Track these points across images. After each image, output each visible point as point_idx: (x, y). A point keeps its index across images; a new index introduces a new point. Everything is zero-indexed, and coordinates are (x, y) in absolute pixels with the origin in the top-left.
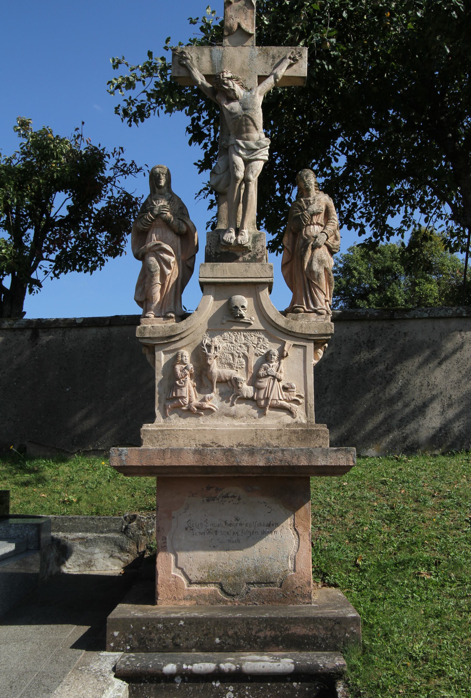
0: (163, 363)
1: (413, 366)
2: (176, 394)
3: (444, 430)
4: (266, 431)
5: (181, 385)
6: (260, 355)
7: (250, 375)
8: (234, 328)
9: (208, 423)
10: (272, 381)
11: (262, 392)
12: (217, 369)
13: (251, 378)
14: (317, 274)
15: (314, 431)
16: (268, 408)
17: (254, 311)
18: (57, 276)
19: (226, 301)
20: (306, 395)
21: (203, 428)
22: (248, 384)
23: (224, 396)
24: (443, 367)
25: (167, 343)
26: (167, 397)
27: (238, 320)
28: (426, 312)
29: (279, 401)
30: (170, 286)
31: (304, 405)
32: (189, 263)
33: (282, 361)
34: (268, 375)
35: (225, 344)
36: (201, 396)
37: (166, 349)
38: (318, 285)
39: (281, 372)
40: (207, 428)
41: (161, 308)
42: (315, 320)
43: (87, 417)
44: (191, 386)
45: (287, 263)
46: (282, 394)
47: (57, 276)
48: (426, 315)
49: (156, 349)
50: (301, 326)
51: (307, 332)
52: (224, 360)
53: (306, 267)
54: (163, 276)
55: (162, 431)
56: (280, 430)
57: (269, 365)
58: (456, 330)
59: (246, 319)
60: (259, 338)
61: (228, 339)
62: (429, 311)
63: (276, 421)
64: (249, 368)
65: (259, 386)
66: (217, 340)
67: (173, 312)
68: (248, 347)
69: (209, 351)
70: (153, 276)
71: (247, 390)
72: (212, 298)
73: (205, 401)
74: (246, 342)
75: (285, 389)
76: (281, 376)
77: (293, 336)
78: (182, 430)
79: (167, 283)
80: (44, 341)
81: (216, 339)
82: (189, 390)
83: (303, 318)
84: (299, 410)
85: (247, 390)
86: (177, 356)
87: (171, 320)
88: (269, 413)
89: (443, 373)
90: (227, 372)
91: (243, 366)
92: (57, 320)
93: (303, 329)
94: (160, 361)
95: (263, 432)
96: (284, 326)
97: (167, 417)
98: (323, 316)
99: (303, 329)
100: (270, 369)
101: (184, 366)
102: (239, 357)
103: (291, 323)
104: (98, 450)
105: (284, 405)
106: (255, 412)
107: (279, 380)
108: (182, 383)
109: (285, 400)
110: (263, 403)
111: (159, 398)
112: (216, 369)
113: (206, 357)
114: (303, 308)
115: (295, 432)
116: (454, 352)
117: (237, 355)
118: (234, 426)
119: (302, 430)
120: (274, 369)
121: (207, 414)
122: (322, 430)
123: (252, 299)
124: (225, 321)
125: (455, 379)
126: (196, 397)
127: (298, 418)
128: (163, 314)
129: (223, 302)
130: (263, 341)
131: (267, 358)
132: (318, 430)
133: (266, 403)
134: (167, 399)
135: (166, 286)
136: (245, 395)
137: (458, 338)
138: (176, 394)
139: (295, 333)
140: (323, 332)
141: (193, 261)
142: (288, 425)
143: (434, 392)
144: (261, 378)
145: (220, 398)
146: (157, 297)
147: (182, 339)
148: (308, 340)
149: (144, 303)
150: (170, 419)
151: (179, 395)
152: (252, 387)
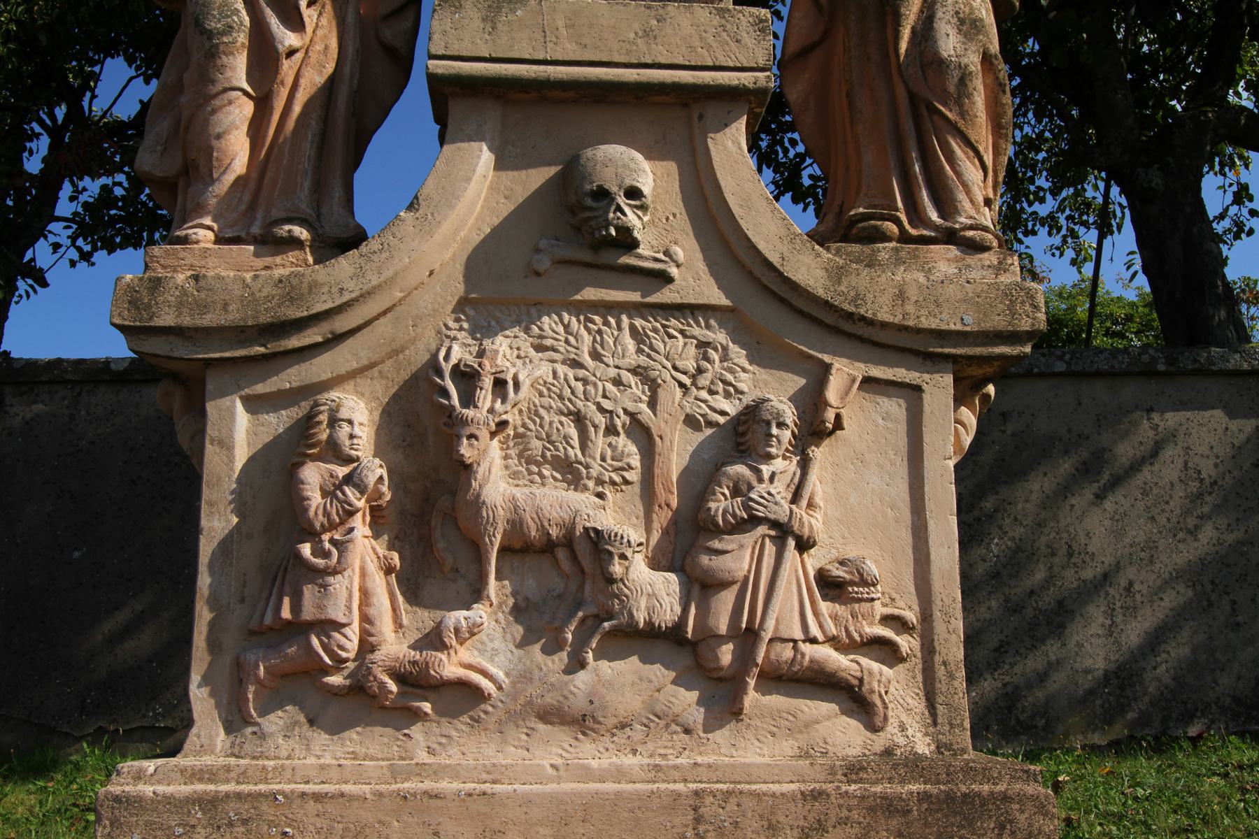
0: (241, 455)
1: (1027, 501)
2: (296, 608)
3: (1123, 677)
4: (748, 803)
5: (320, 562)
6: (710, 424)
7: (662, 518)
8: (590, 294)
9: (451, 757)
10: (770, 549)
11: (725, 602)
12: (502, 486)
13: (665, 532)
14: (956, 74)
15: (984, 800)
16: (752, 682)
17: (682, 222)
18: (86, 257)
19: (551, 171)
20: (926, 616)
21: (428, 785)
22: (655, 564)
23: (536, 621)
24: (1108, 505)
25: (264, 357)
26: (253, 625)
27: (607, 256)
28: (1061, 358)
29: (807, 648)
30: (297, 109)
31: (917, 662)
32: (390, 33)
33: (818, 453)
34: (754, 521)
35: (544, 370)
36: (419, 619)
37: (260, 388)
38: (961, 124)
39: (811, 505)
40: (445, 785)
41: (252, 207)
42: (952, 270)
43: (127, 631)
44: (373, 567)
45: (804, 53)
46: (816, 614)
47: (86, 257)
48: (1060, 367)
49: (210, 387)
50: (901, 296)
51: (925, 323)
52: (537, 445)
53: (903, 46)
54: (265, 58)
55: (210, 803)
56: (817, 795)
57: (758, 472)
58: (1137, 407)
59: (647, 252)
60: (703, 345)
61: (561, 346)
62: (1067, 357)
63: (788, 747)
64: (659, 487)
65: (707, 571)
66: (505, 350)
67: (302, 222)
68: (653, 386)
69: (468, 400)
70: (212, 54)
71: (653, 592)
72: (485, 157)
73: (443, 647)
74: (643, 360)
75: (830, 586)
76: (813, 522)
77: (860, 339)
78: (318, 797)
79: (284, 93)
80: (19, 419)
81: (502, 345)
82: (360, 588)
83: (899, 262)
84: (896, 687)
85: (653, 592)
86: (309, 421)
87: (292, 256)
88: (756, 706)
89: (1107, 523)
90: (555, 502)
91: (633, 476)
92: (59, 361)
93: (910, 308)
94: (227, 445)
95: (731, 806)
96: (821, 292)
97: (247, 721)
98: (990, 258)
99: (910, 308)
100: (762, 488)
101: (342, 471)
102: (611, 430)
103: (854, 280)
104: (153, 727)
105: (831, 667)
106: (686, 701)
107: (804, 545)
108: (326, 555)
109: (833, 641)
110: (726, 654)
111: (212, 625)
112: (499, 483)
113: (452, 426)
114: (897, 221)
115: (889, 806)
116: (1135, 467)
117: (601, 420)
118: (587, 774)
119: (924, 797)
120: (781, 490)
121: (448, 712)
122: (1022, 798)
123: (672, 167)
124: (544, 263)
125: (1141, 537)
126: (398, 625)
127: (892, 728)
128: (256, 230)
129: (538, 177)
130: (725, 358)
131: (744, 435)
132: (1005, 798)
133: (745, 656)
134: (252, 633)
135: (279, 105)
136: (641, 617)
137: (1145, 432)
138: (296, 608)
139: (870, 322)
140: (997, 322)
141: (407, 24)
142: (854, 770)
143: (1088, 574)
144: (717, 532)
145: (519, 630)
146: (236, 153)
147: (337, 339)
148: (931, 361)
149: (181, 184)
150: (262, 736)
151: (309, 613)
152: (672, 577)
